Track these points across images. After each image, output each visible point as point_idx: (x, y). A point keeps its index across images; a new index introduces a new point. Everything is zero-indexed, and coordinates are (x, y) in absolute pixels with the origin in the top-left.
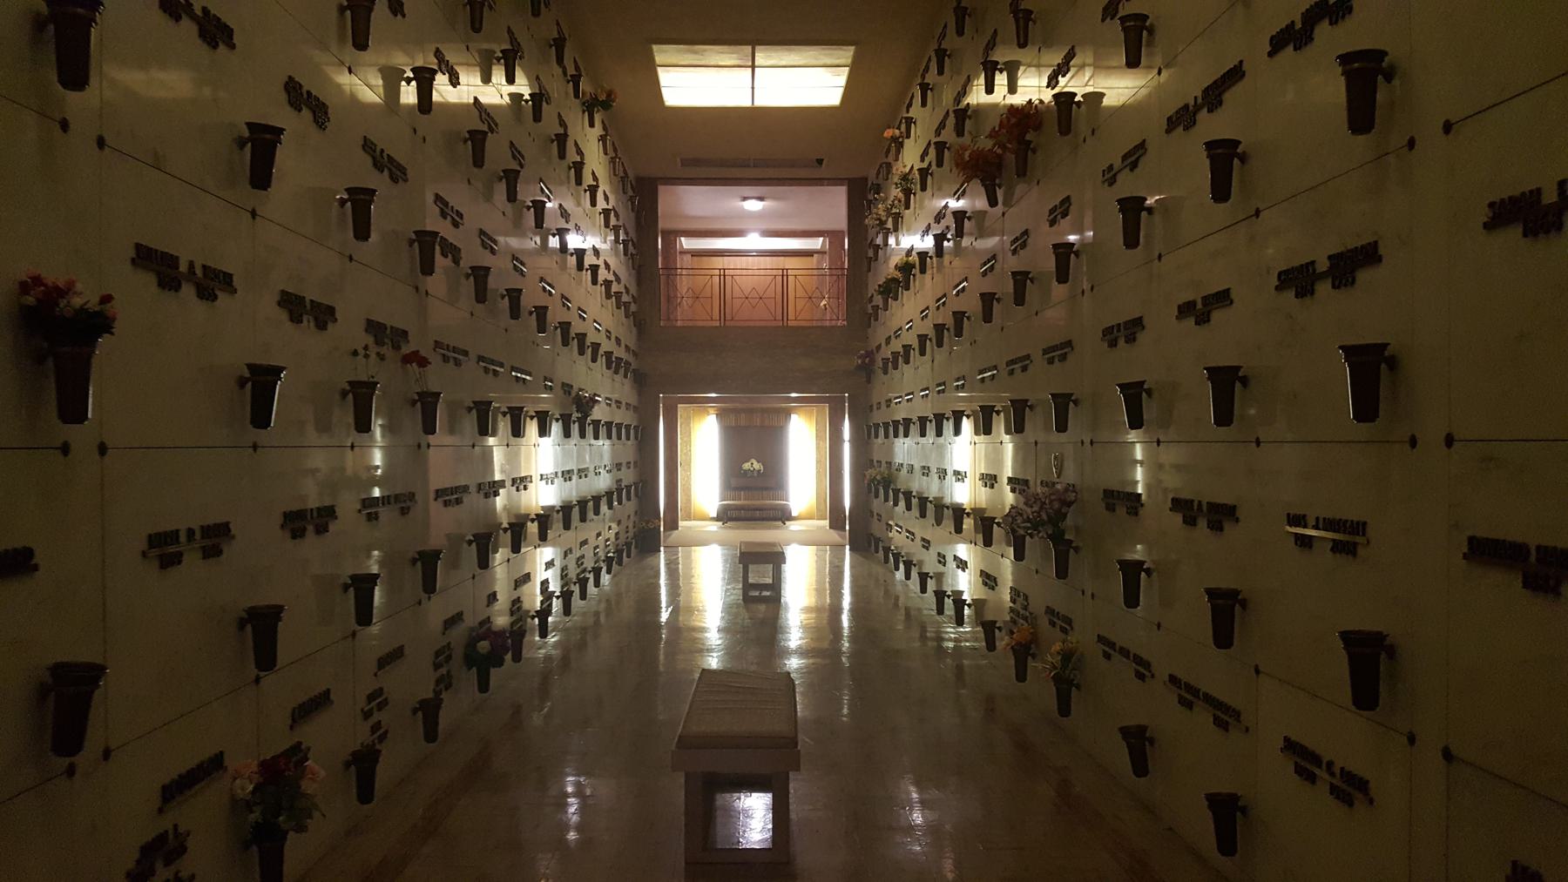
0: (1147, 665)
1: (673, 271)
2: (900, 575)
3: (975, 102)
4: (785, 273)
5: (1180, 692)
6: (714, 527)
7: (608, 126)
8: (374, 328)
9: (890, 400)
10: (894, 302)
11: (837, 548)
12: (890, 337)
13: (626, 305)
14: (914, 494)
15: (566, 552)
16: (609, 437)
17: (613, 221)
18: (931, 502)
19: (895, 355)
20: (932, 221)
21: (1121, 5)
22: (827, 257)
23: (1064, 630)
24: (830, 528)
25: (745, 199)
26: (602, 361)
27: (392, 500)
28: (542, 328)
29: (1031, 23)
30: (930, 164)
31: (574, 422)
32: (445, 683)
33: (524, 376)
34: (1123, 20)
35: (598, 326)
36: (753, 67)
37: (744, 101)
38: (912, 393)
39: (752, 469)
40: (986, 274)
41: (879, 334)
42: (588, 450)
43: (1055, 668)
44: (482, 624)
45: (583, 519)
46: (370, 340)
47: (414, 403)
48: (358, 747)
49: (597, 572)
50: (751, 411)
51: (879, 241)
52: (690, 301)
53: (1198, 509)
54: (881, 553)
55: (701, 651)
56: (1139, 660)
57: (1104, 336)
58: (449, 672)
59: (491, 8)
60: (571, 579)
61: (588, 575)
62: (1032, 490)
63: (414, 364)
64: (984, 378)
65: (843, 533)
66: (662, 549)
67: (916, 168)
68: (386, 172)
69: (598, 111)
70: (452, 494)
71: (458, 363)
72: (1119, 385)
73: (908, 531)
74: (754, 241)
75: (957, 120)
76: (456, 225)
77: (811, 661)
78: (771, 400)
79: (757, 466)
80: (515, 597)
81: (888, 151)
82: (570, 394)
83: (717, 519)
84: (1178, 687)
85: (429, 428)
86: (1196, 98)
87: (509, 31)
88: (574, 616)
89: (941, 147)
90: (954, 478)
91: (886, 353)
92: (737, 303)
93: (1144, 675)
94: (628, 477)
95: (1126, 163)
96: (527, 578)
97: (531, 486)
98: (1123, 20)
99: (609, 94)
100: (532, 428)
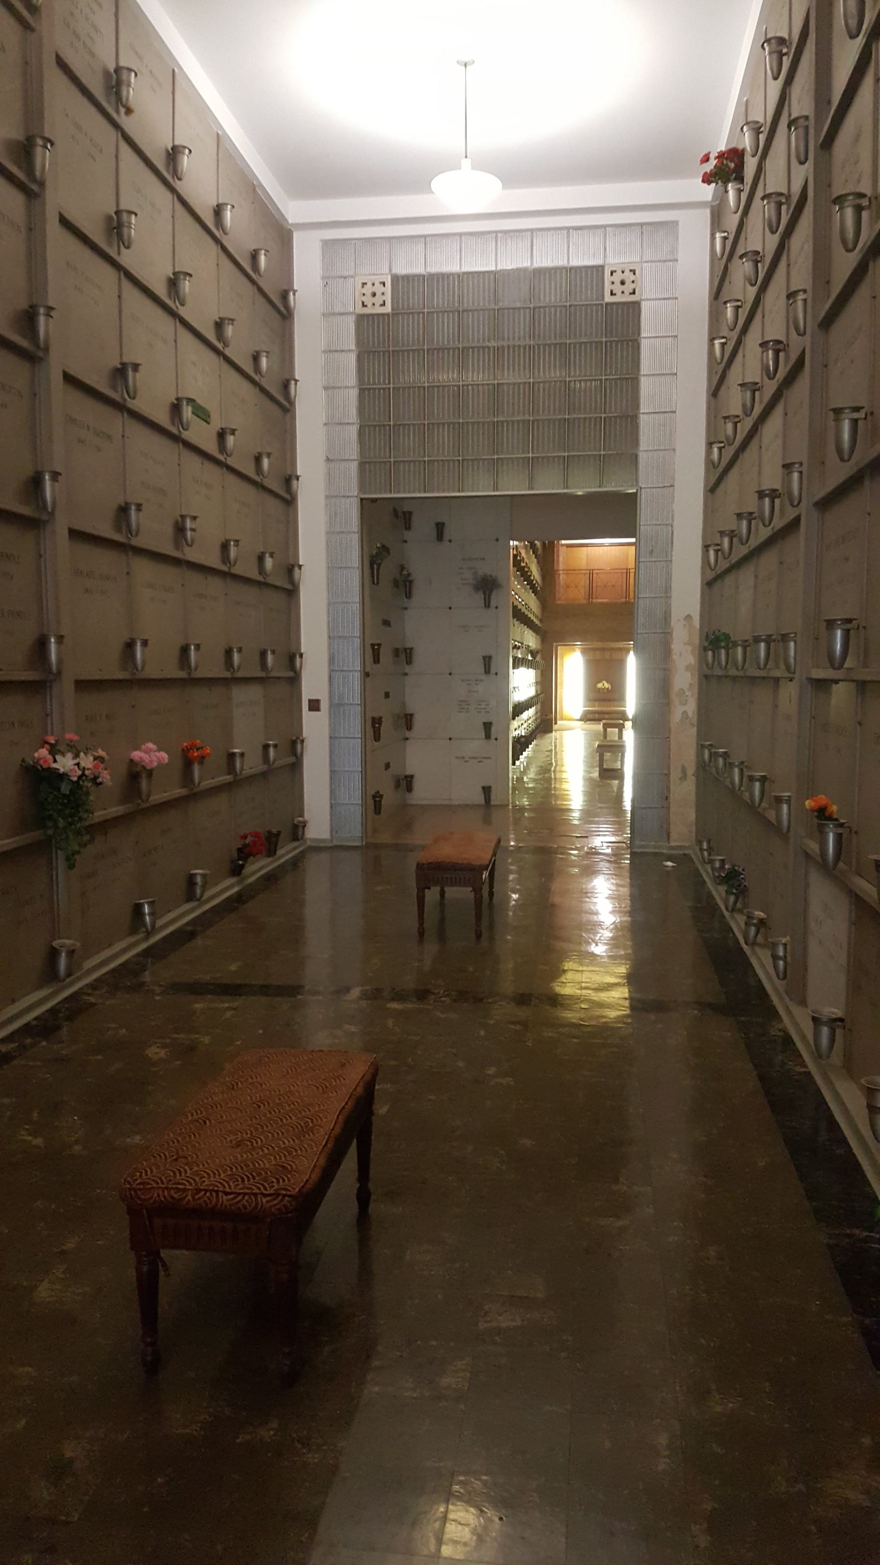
50: (603, 649)
79: (607, 685)
83: (581, 720)
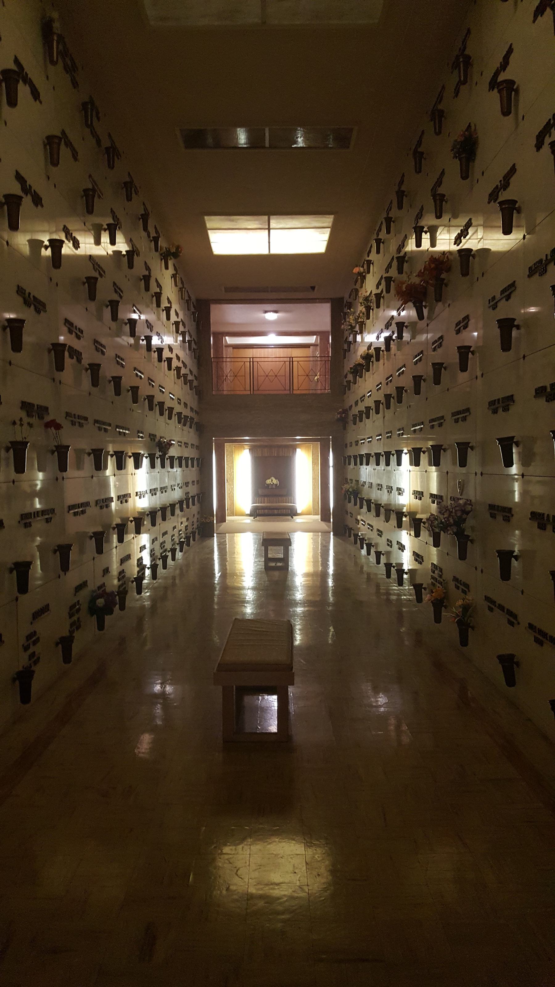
0: (515, 616)
1: (221, 360)
2: (364, 552)
3: (410, 250)
4: (291, 360)
5: (535, 634)
6: (248, 520)
7: (177, 268)
8: (26, 406)
9: (358, 441)
10: (360, 379)
11: (325, 533)
12: (358, 401)
13: (191, 382)
14: (372, 501)
15: (153, 540)
16: (180, 466)
17: (181, 329)
18: (383, 507)
19: (361, 412)
20: (383, 327)
21: (500, 193)
22: (319, 348)
23: (464, 592)
24: (321, 520)
25: (266, 312)
26: (175, 418)
27: (40, 514)
28: (135, 400)
29: (444, 202)
30: (382, 291)
31: (157, 458)
32: (76, 625)
33: (124, 431)
34: (501, 203)
35: (172, 396)
36: (269, 229)
37: (263, 250)
38: (371, 437)
39: (272, 483)
40: (417, 363)
41: (351, 399)
42: (167, 475)
43: (458, 616)
44: (99, 588)
45: (164, 519)
46: (23, 414)
47: (53, 452)
48: (21, 669)
49: (173, 551)
50: (270, 447)
51: (351, 338)
52: (232, 378)
53: (547, 520)
54: (352, 537)
55: (237, 602)
56: (510, 613)
57: (490, 406)
58: (78, 619)
59: (99, 197)
60: (157, 556)
61: (168, 554)
62: (444, 503)
63: (53, 428)
64: (415, 430)
65: (329, 524)
66: (215, 535)
67: (373, 293)
68: (32, 307)
69: (171, 259)
70: (79, 508)
71: (81, 425)
72: (498, 439)
73: (369, 524)
74: (272, 339)
75: (398, 264)
76: (78, 337)
77: (306, 609)
78: (284, 440)
79: (275, 481)
80: (121, 570)
81: (356, 282)
82: (154, 440)
83: (250, 515)
84: (534, 631)
85: (63, 467)
86: (547, 255)
87: (112, 211)
88: (159, 579)
89: (389, 280)
90: (397, 493)
91: (355, 411)
92: (261, 379)
93: (513, 622)
94: (193, 490)
95: (503, 295)
96: (128, 557)
97: (130, 500)
98: (501, 203)
99: (178, 247)
100: (130, 462)
